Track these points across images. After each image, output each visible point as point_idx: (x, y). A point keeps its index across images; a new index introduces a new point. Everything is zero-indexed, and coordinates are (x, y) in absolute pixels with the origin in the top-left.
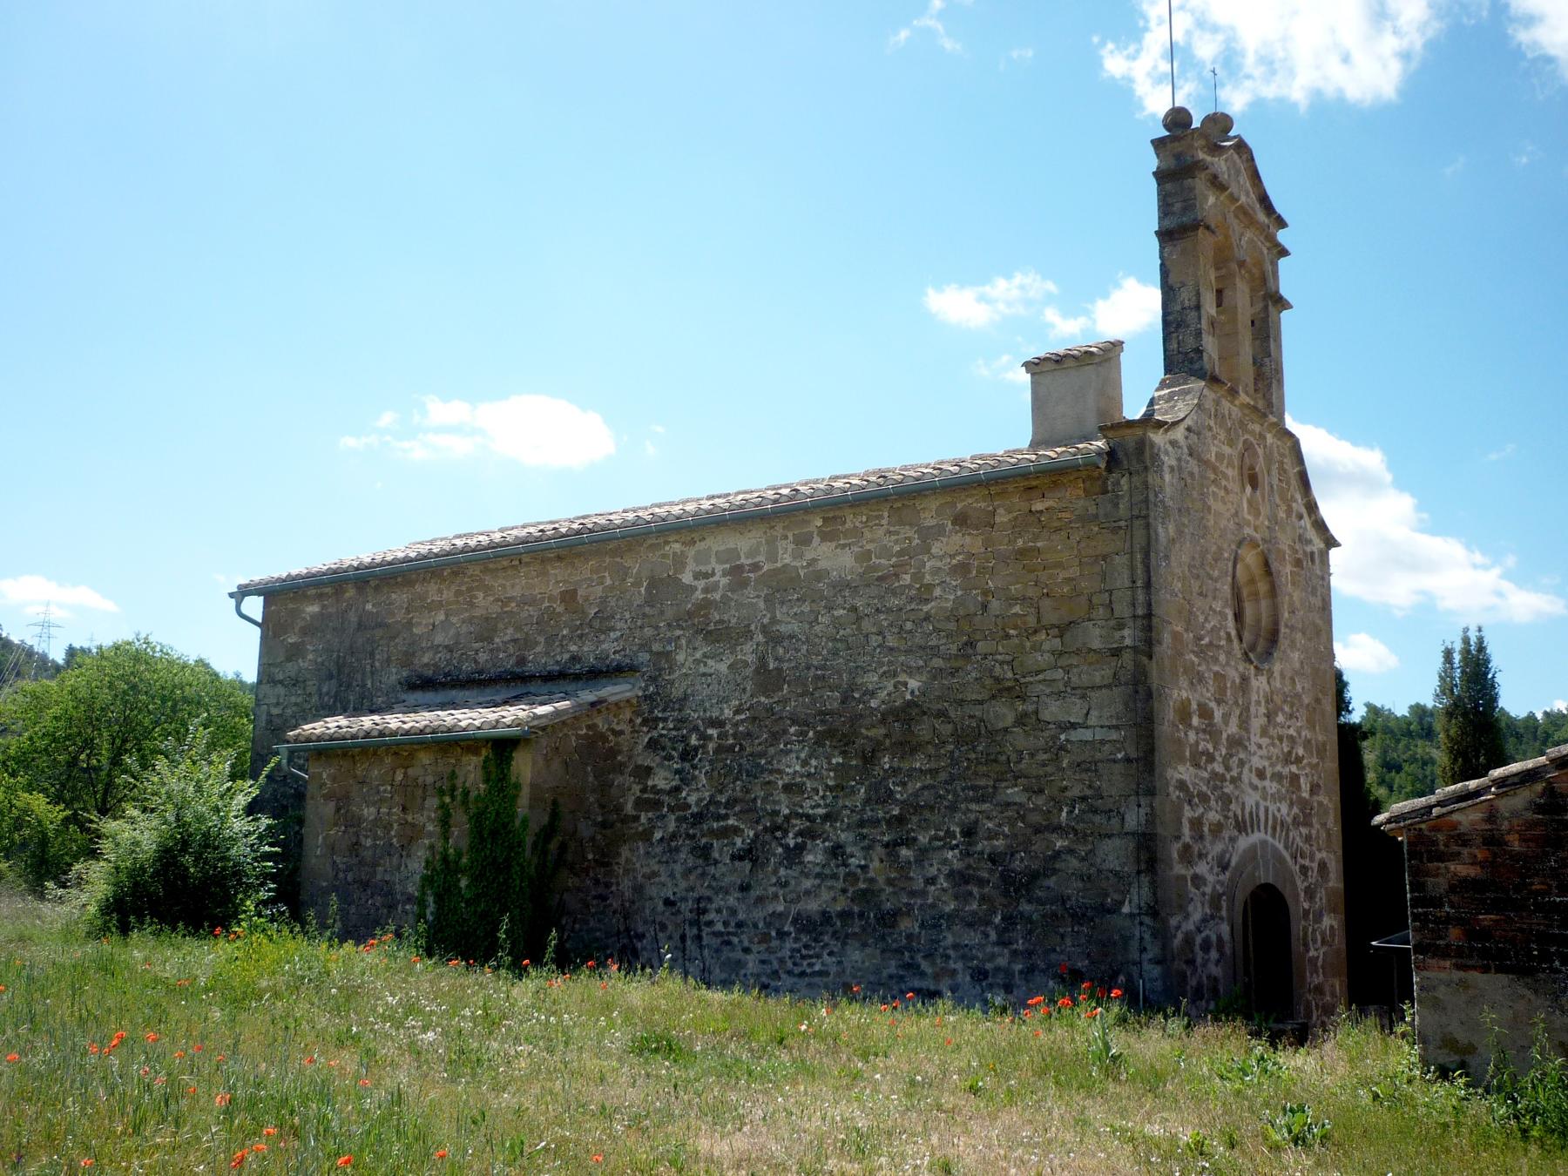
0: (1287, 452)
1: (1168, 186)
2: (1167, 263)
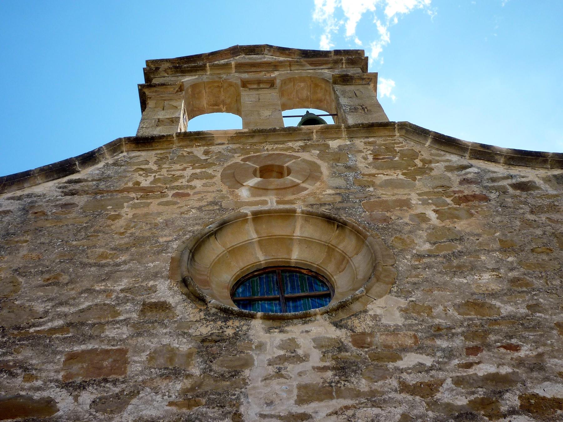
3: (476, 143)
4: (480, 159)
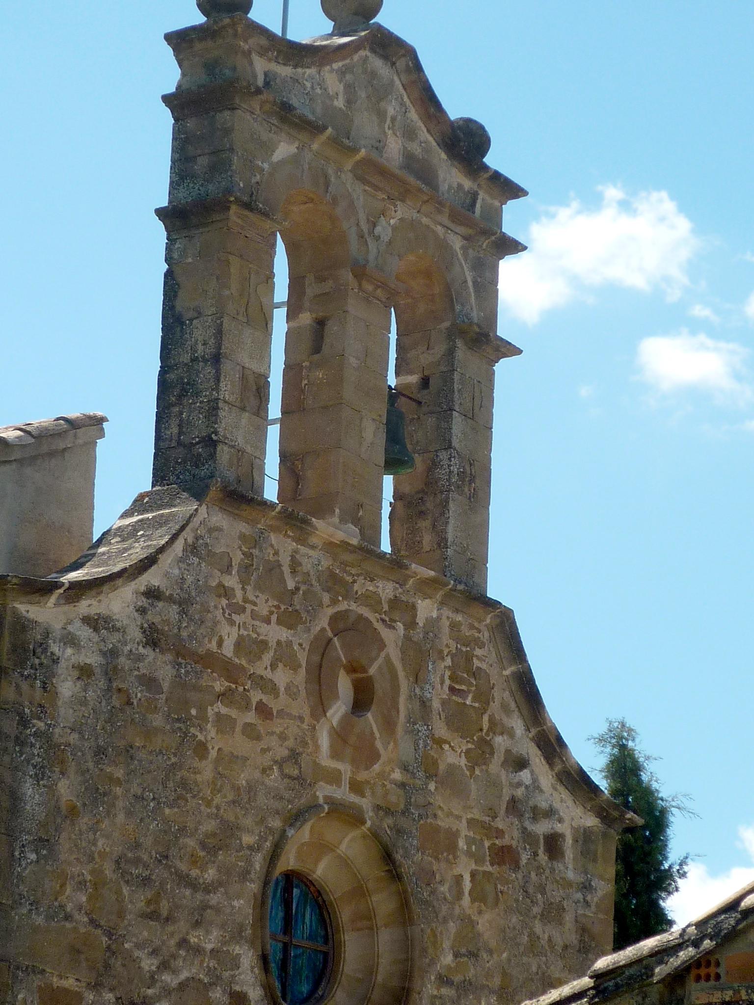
0: (485, 635)
1: (191, 124)
2: (177, 270)
3: (556, 729)
4: (541, 750)
